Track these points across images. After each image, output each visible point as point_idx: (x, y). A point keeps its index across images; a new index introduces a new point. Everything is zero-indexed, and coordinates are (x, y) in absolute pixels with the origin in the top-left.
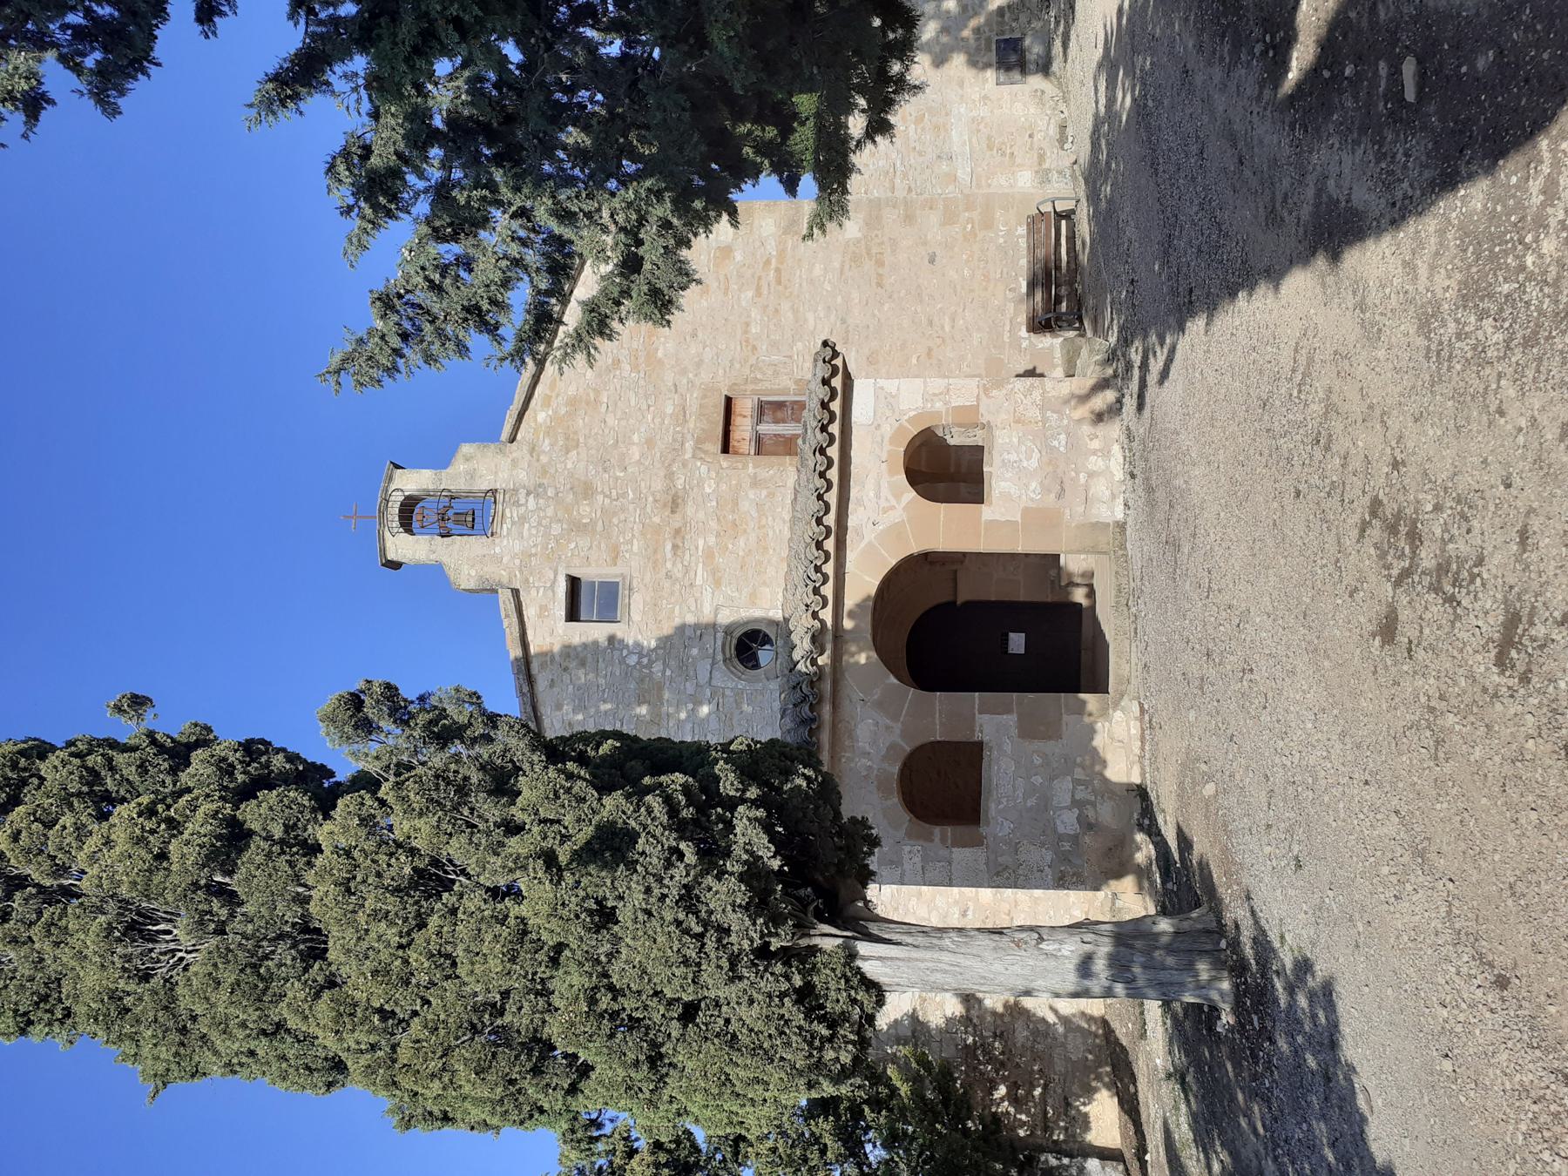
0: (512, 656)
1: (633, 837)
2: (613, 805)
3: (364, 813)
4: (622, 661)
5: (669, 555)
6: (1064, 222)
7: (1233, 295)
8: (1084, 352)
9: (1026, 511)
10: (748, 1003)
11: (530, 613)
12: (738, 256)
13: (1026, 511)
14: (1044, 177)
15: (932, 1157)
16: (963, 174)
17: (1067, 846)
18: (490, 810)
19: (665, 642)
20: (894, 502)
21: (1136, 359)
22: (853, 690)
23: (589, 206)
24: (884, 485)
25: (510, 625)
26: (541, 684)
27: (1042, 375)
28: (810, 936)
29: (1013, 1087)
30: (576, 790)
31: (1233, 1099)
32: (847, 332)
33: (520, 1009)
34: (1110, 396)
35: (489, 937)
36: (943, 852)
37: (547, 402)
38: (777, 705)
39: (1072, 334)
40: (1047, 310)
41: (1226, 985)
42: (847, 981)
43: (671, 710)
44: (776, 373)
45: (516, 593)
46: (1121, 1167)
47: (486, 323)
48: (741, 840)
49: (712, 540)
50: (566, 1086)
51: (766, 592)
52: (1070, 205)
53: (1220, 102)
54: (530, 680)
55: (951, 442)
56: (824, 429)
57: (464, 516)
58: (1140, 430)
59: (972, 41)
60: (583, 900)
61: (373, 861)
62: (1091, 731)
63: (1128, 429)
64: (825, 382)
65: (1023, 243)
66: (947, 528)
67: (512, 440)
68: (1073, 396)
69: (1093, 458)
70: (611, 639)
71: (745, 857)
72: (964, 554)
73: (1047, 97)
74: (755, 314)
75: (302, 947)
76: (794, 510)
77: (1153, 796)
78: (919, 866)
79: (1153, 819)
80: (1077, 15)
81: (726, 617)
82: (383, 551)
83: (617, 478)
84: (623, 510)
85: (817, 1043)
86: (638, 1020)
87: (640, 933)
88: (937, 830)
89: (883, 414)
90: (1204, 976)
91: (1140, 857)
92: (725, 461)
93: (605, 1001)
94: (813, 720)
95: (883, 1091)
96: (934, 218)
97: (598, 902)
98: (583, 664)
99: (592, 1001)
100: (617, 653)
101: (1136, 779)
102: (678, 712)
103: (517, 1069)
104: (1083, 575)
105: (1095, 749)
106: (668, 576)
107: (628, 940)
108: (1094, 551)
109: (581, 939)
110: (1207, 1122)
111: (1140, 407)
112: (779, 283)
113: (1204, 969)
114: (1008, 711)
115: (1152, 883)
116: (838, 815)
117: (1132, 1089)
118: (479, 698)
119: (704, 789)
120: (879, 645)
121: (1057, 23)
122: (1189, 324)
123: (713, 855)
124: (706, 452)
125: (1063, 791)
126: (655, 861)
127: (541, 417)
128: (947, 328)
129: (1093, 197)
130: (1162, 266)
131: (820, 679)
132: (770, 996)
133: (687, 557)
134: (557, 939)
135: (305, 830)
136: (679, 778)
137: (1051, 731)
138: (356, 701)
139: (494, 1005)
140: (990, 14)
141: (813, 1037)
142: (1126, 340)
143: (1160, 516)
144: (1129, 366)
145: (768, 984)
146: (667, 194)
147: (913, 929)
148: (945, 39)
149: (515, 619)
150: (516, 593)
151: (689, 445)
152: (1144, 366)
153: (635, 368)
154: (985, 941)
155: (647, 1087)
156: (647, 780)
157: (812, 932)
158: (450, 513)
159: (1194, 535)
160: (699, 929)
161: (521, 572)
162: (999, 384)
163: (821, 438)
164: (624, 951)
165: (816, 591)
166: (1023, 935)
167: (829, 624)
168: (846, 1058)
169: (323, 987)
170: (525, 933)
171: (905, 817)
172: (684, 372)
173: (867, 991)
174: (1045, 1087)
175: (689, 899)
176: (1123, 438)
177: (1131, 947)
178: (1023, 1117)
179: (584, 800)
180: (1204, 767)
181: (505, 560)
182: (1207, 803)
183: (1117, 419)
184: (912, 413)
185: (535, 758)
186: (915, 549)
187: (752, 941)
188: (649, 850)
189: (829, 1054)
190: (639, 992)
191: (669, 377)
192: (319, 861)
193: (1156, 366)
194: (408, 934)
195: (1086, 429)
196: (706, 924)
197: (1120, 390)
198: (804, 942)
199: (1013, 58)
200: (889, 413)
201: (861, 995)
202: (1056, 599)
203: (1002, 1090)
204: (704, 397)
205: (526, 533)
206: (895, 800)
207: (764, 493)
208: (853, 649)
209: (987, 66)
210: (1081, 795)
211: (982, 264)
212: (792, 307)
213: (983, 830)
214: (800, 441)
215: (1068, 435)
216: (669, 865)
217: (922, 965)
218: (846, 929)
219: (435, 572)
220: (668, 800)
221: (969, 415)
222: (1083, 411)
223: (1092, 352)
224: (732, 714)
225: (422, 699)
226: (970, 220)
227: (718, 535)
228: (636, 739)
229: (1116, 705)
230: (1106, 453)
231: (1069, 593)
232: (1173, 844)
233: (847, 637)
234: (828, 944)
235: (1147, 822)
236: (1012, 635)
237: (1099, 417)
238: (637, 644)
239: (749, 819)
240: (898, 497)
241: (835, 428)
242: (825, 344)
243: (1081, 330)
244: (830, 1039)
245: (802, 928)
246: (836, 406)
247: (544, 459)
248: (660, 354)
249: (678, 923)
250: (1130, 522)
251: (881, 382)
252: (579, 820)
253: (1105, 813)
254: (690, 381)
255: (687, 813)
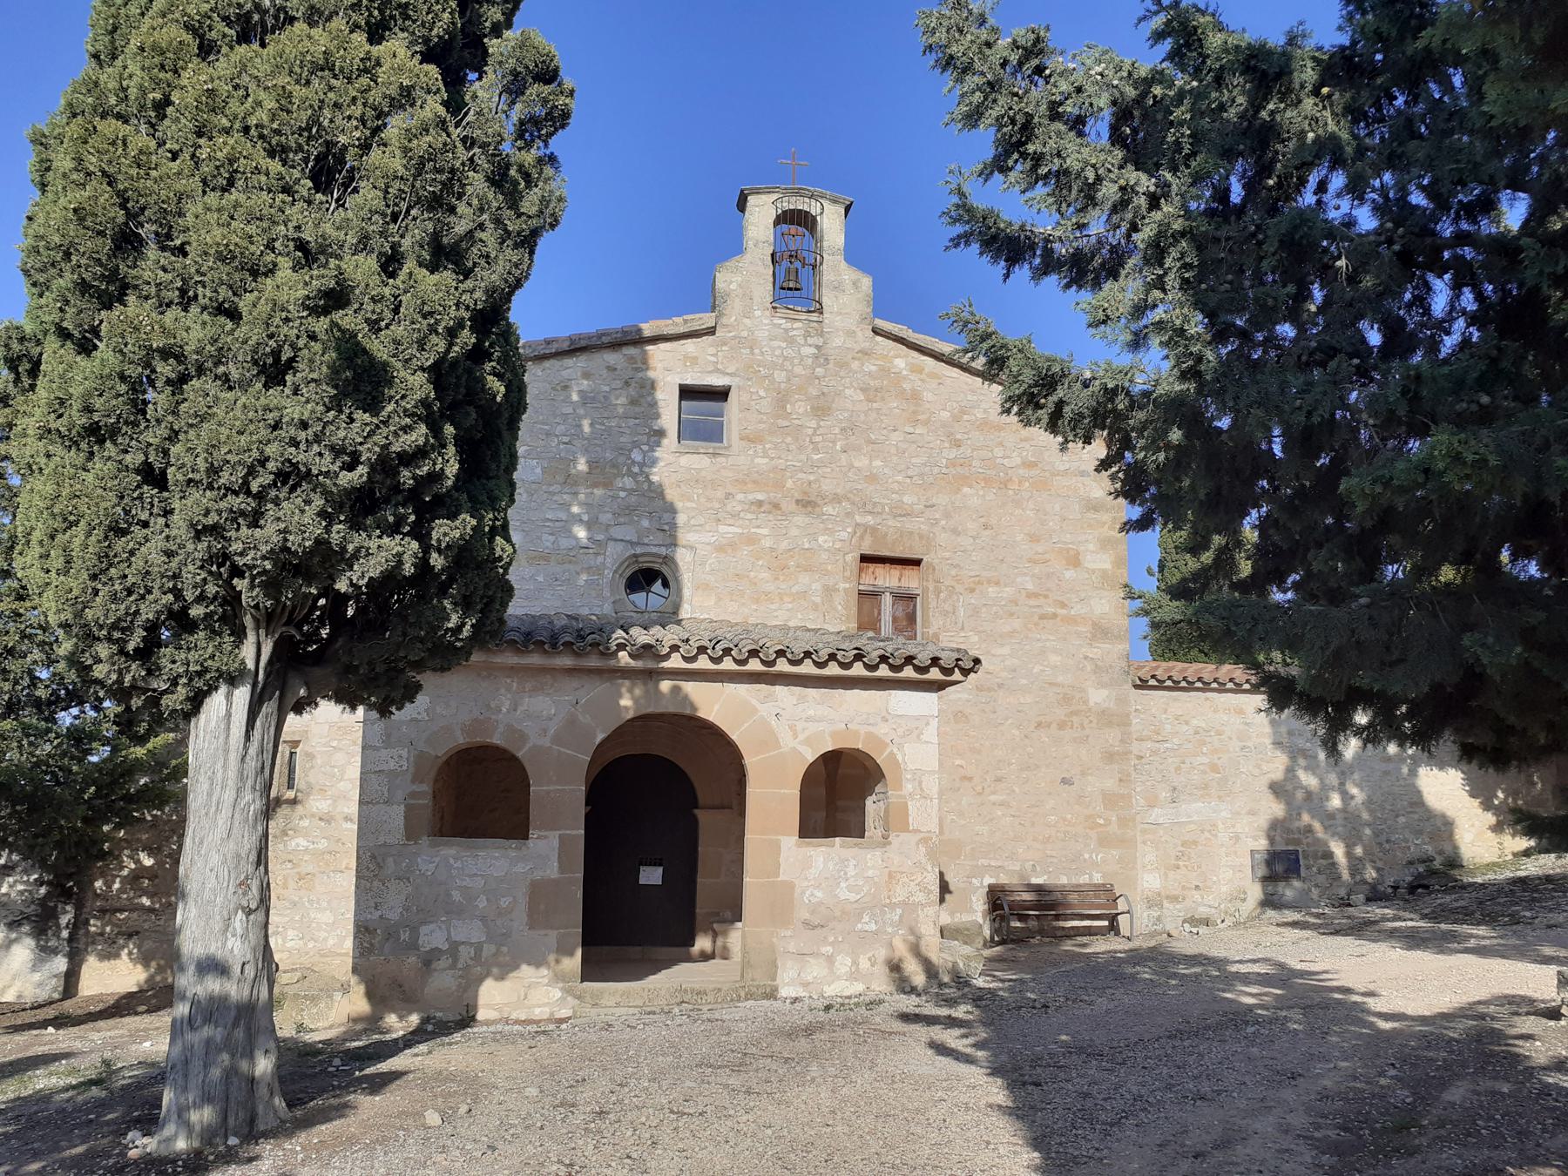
0: (644, 326)
1: (373, 406)
2: (415, 385)
3: (418, 92)
4: (636, 445)
5: (751, 497)
6: (1106, 923)
7: (1037, 1143)
8: (968, 950)
9: (790, 886)
10: (165, 549)
11: (689, 345)
12: (1069, 574)
13: (790, 886)
14: (1153, 902)
15: (58, 783)
16: (1156, 814)
17: (405, 936)
18: (414, 235)
19: (657, 492)
20: (801, 737)
21: (960, 1012)
22: (594, 690)
23: (1172, 280)
24: (821, 727)
25: (676, 325)
26: (611, 358)
27: (942, 900)
28: (257, 628)
29: (151, 874)
30: (434, 339)
31: (36, 1156)
32: (989, 690)
33: (165, 270)
34: (919, 979)
35: (252, 229)
36: (400, 795)
37: (918, 370)
38: (585, 611)
39: (987, 932)
40: (1013, 905)
41: (181, 1144)
42: (200, 674)
43: (582, 497)
44: (946, 614)
45: (711, 331)
46: (56, 996)
47: (1008, 154)
48: (373, 544)
49: (767, 543)
50: (65, 324)
51: (708, 598)
52: (1125, 930)
53: (1265, 1125)
54: (616, 345)
55: (869, 802)
56: (884, 659)
57: (795, 281)
58: (879, 1018)
59: (1297, 824)
60: (293, 346)
61: (354, 99)
62: (538, 964)
63: (881, 1002)
64: (935, 661)
65: (1084, 879)
66: (772, 797)
67: (876, 331)
68: (919, 938)
69: (849, 961)
70: (661, 433)
71: (350, 548)
72: (742, 814)
73: (1238, 904)
74: (1008, 591)
75: (256, 17)
76: (797, 628)
77: (457, 1036)
78: (385, 767)
79: (431, 1036)
80: (1330, 939)
81: (683, 557)
82: (757, 192)
83: (834, 442)
84: (801, 448)
85: (117, 635)
86: (144, 413)
87: (251, 414)
88: (426, 788)
89: (900, 727)
90: (194, 1116)
91: (391, 1019)
92: (852, 558)
93: (165, 369)
94: (554, 646)
95: (142, 728)
96: (1110, 784)
97: (292, 360)
98: (633, 402)
99: (166, 353)
100: (645, 438)
101: (481, 1015)
102: (580, 504)
103: (84, 261)
104: (725, 948)
105: (517, 967)
106: (729, 496)
107: (243, 399)
108: (746, 964)
109: (245, 342)
110: (30, 1118)
111: (906, 1018)
112: (1042, 617)
113: (203, 1116)
114: (562, 869)
115: (357, 1036)
116: (419, 666)
117: (142, 1008)
118: (552, 226)
119: (439, 500)
120: (643, 721)
121: (1318, 916)
122: (999, 1081)
123: (360, 507)
124: (862, 538)
125: (468, 931)
126: (341, 434)
127: (900, 363)
128: (993, 798)
129: (1137, 957)
130: (1065, 1045)
131: (602, 654)
132: (176, 576)
133: (749, 516)
134: (245, 311)
135: (402, 30)
136: (452, 469)
137: (538, 915)
138: (547, 75)
139: (169, 237)
140: (1326, 844)
141: (123, 630)
142: (980, 999)
143: (778, 1044)
144: (951, 1002)
145: (192, 575)
146: (1192, 386)
147: (268, 757)
148: (1300, 795)
149: (682, 330)
150: (711, 331)
151: (870, 520)
152: (952, 1022)
153: (952, 463)
154: (249, 843)
155: (61, 425)
156: (449, 430)
157: (262, 632)
158: (798, 264)
159: (748, 1092)
160: (255, 487)
161: (734, 338)
162: (932, 855)
163: (874, 656)
164: (230, 395)
165: (702, 650)
166: (255, 890)
167: (666, 665)
168: (99, 671)
169: (202, 37)
170: (255, 273)
171: (442, 750)
172: (947, 516)
173: (188, 699)
174: (151, 910)
175: (291, 476)
176: (871, 996)
177: (235, 1024)
178: (116, 886)
179: (422, 349)
180: (463, 1109)
181: (747, 321)
182: (420, 1114)
183: (892, 988)
184: (899, 758)
185: (478, 295)
186: (750, 761)
187: (241, 554)
188: (355, 428)
189: (103, 650)
190: (175, 413)
191: (942, 500)
192: (360, 38)
193: (951, 1038)
194: (261, 136)
195: (882, 953)
196: (260, 497)
197: (925, 992)
198: (248, 621)
199: (1279, 868)
200: (900, 731)
201: (182, 691)
202: (699, 918)
203: (148, 862)
204: (921, 537)
205: (776, 343)
206: (461, 740)
207: (818, 600)
208: (637, 692)
209: (1271, 840)
210: (465, 953)
211: (1061, 835)
212: (1014, 631)
213: (425, 841)
214: (871, 634)
215: (876, 933)
216: (337, 451)
217: (219, 765)
218: (268, 675)
219: (735, 246)
220: (420, 453)
221: (896, 821)
222: (901, 950)
223: (969, 958)
224: (551, 551)
225: (552, 159)
226: (1108, 822)
227: (772, 549)
228: (513, 425)
229: (568, 991)
230: (854, 976)
231: (705, 932)
232: (384, 1067)
233: (651, 685)
234: (248, 652)
235: (430, 1028)
236: (660, 870)
237: (895, 967)
238: (654, 462)
239: (399, 555)
240: (808, 742)
241: (884, 671)
242: (977, 661)
243: (991, 943)
244: (122, 652)
245: (267, 620)
246: (908, 672)
247: (855, 365)
248: (966, 490)
249: (263, 462)
250: (777, 1004)
251: (934, 723)
252: (397, 342)
253: (443, 981)
254: (937, 521)
255: (406, 477)
